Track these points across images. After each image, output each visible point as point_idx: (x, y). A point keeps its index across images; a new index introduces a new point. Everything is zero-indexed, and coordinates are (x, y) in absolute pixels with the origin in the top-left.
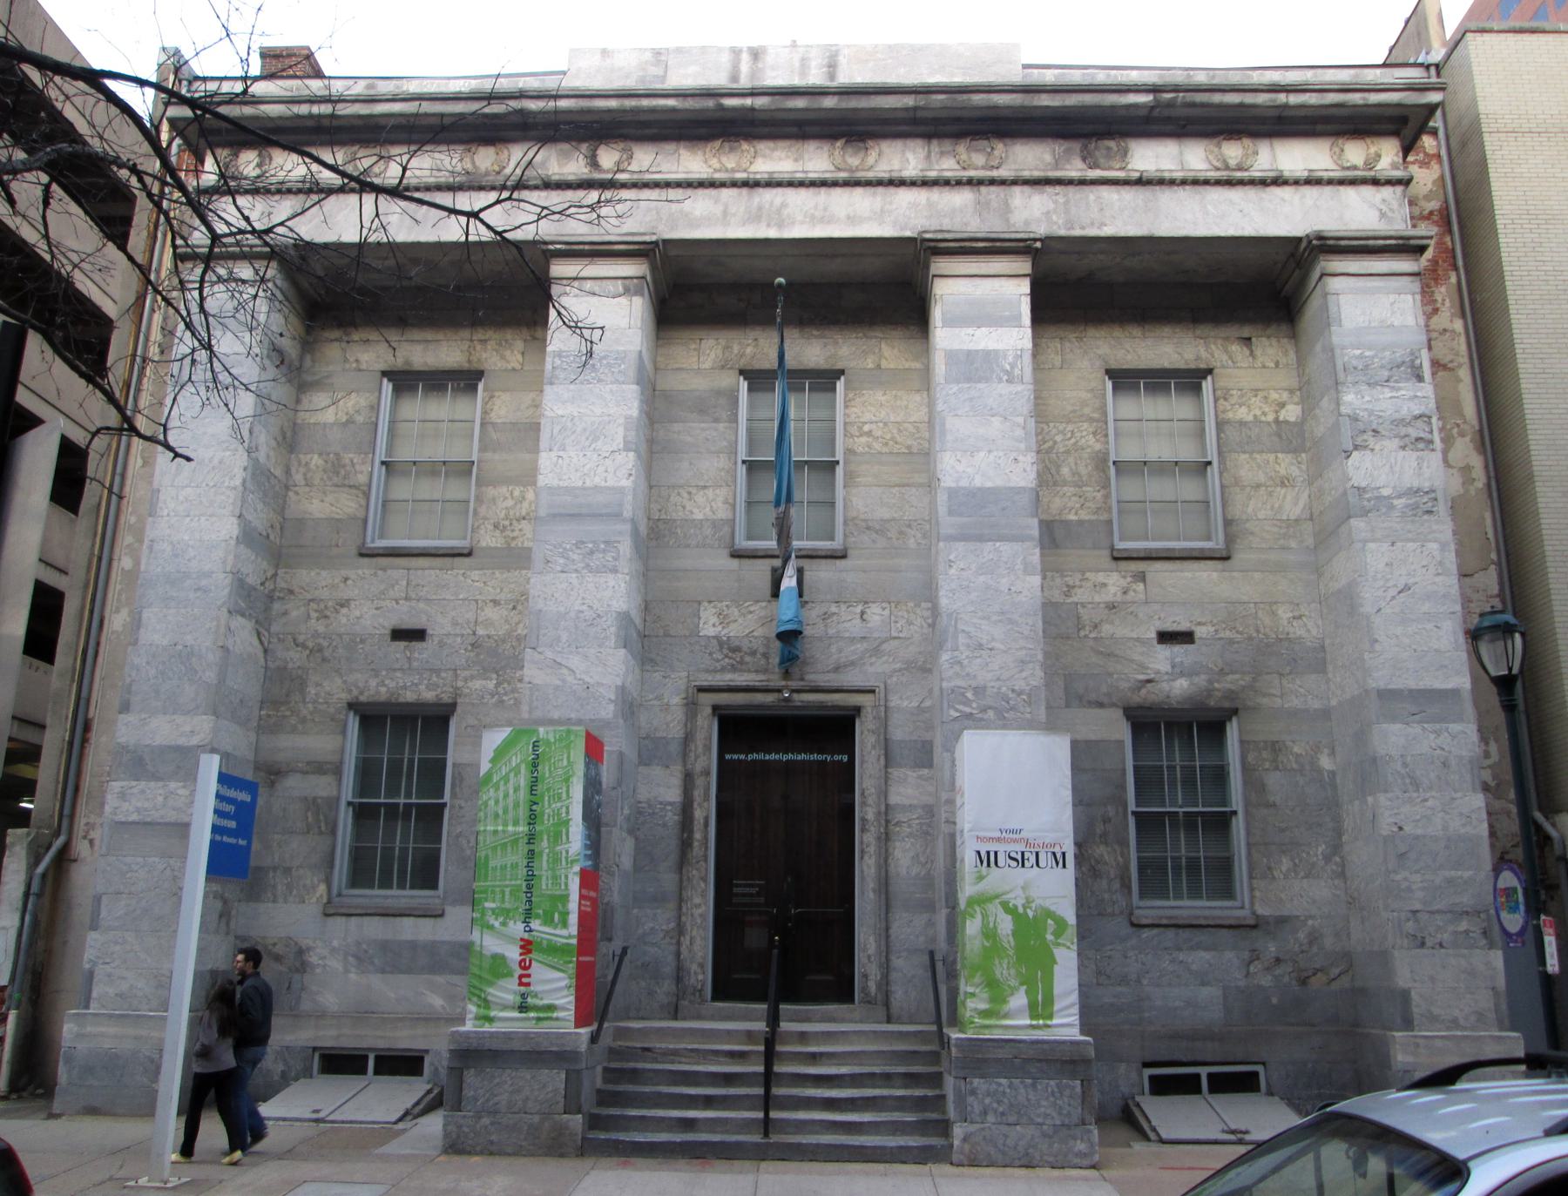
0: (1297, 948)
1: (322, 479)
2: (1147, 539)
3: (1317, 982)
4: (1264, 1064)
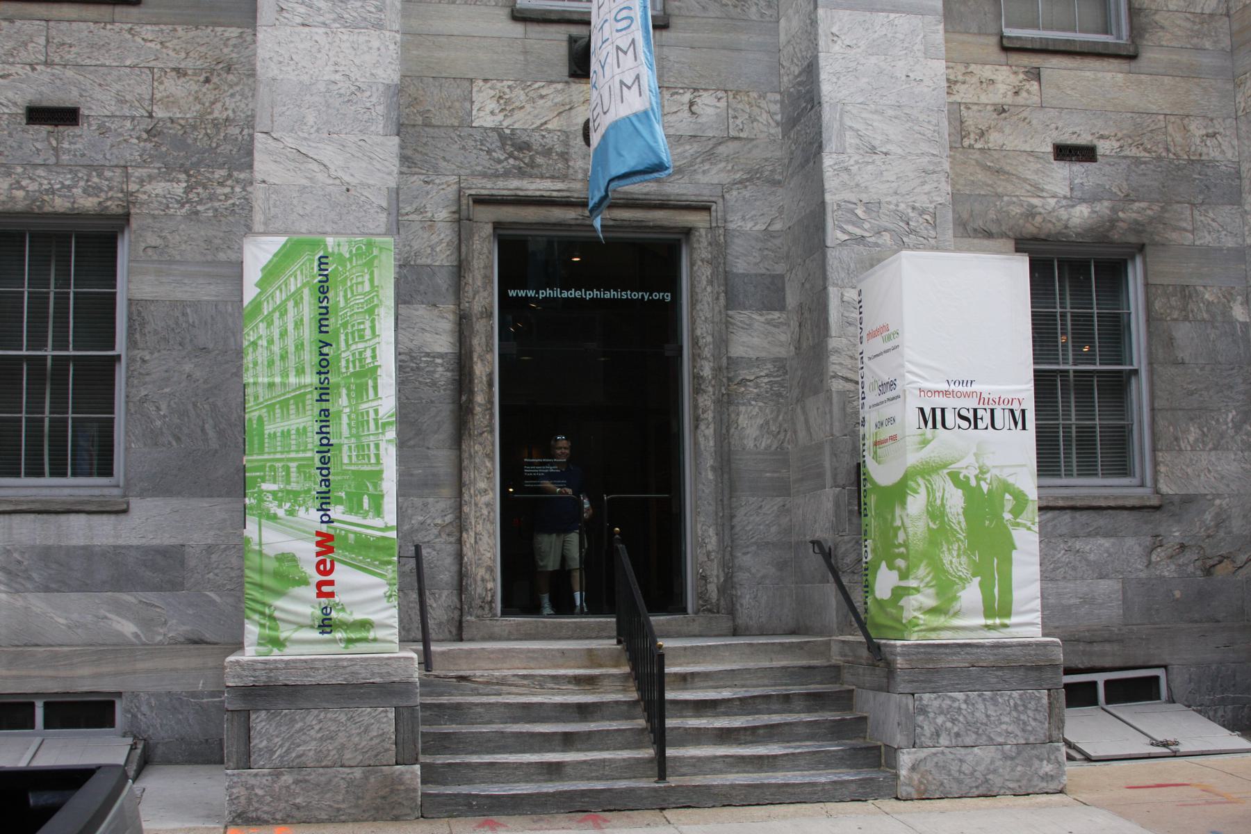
0: (1203, 533)
2: (1037, 27)
3: (1222, 571)
4: (1165, 667)
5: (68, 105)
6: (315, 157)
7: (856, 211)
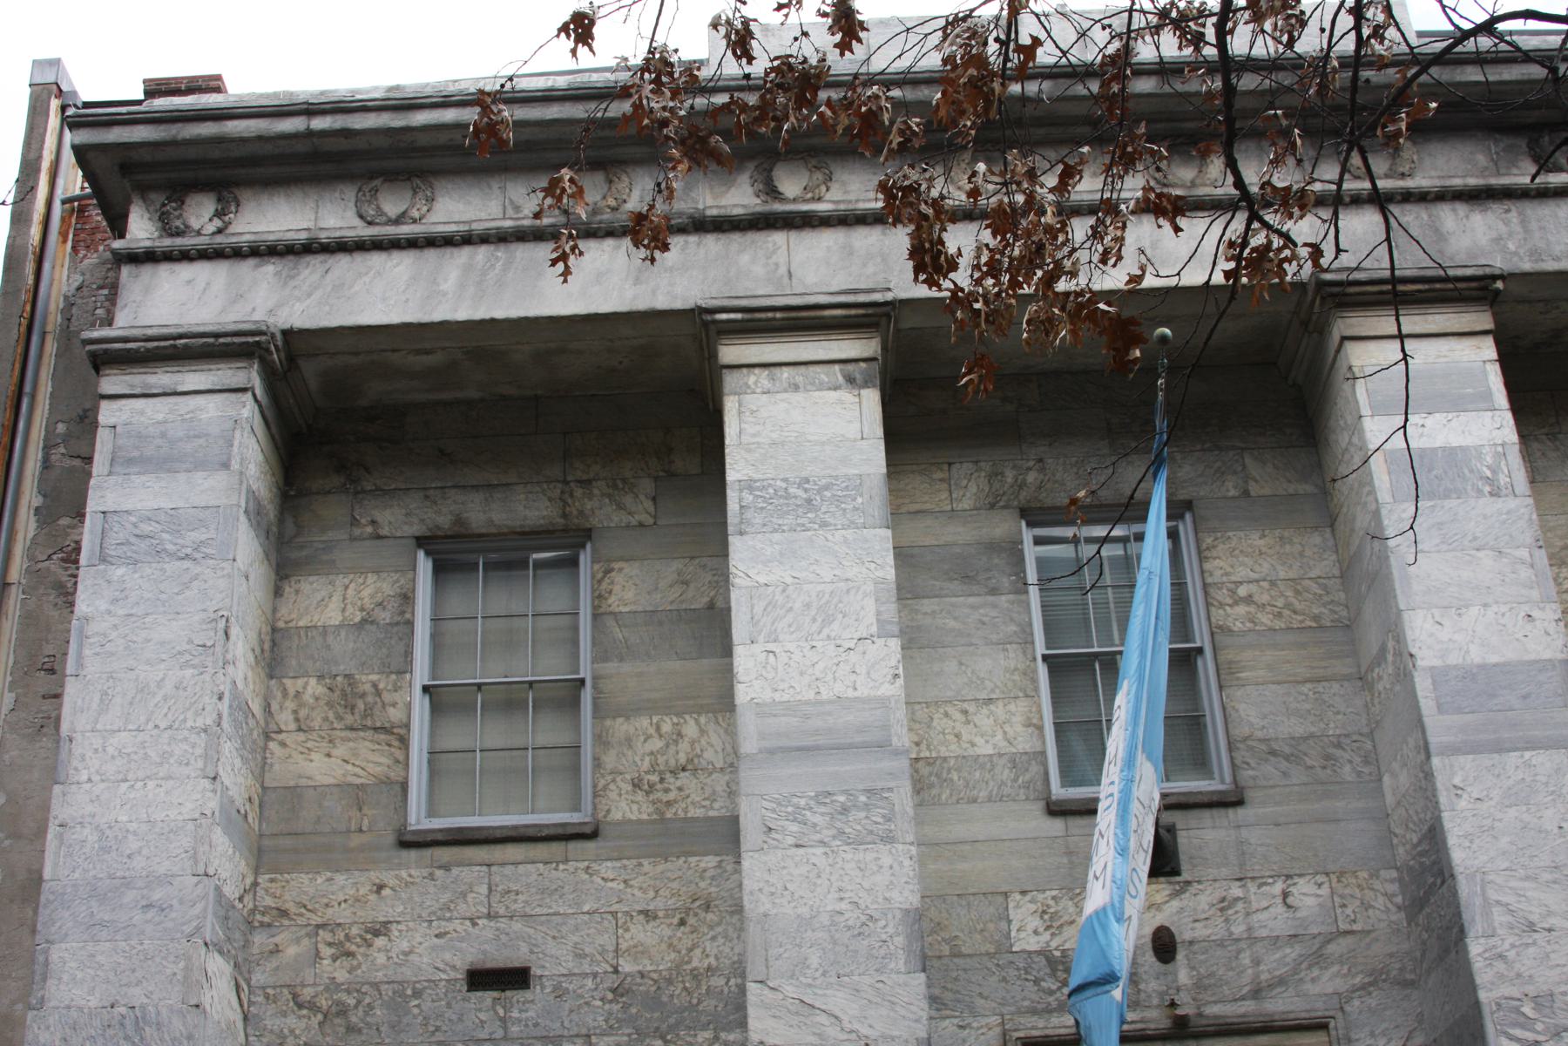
1: (326, 719)
5: (517, 964)
6: (823, 1007)
7: (1523, 1009)
